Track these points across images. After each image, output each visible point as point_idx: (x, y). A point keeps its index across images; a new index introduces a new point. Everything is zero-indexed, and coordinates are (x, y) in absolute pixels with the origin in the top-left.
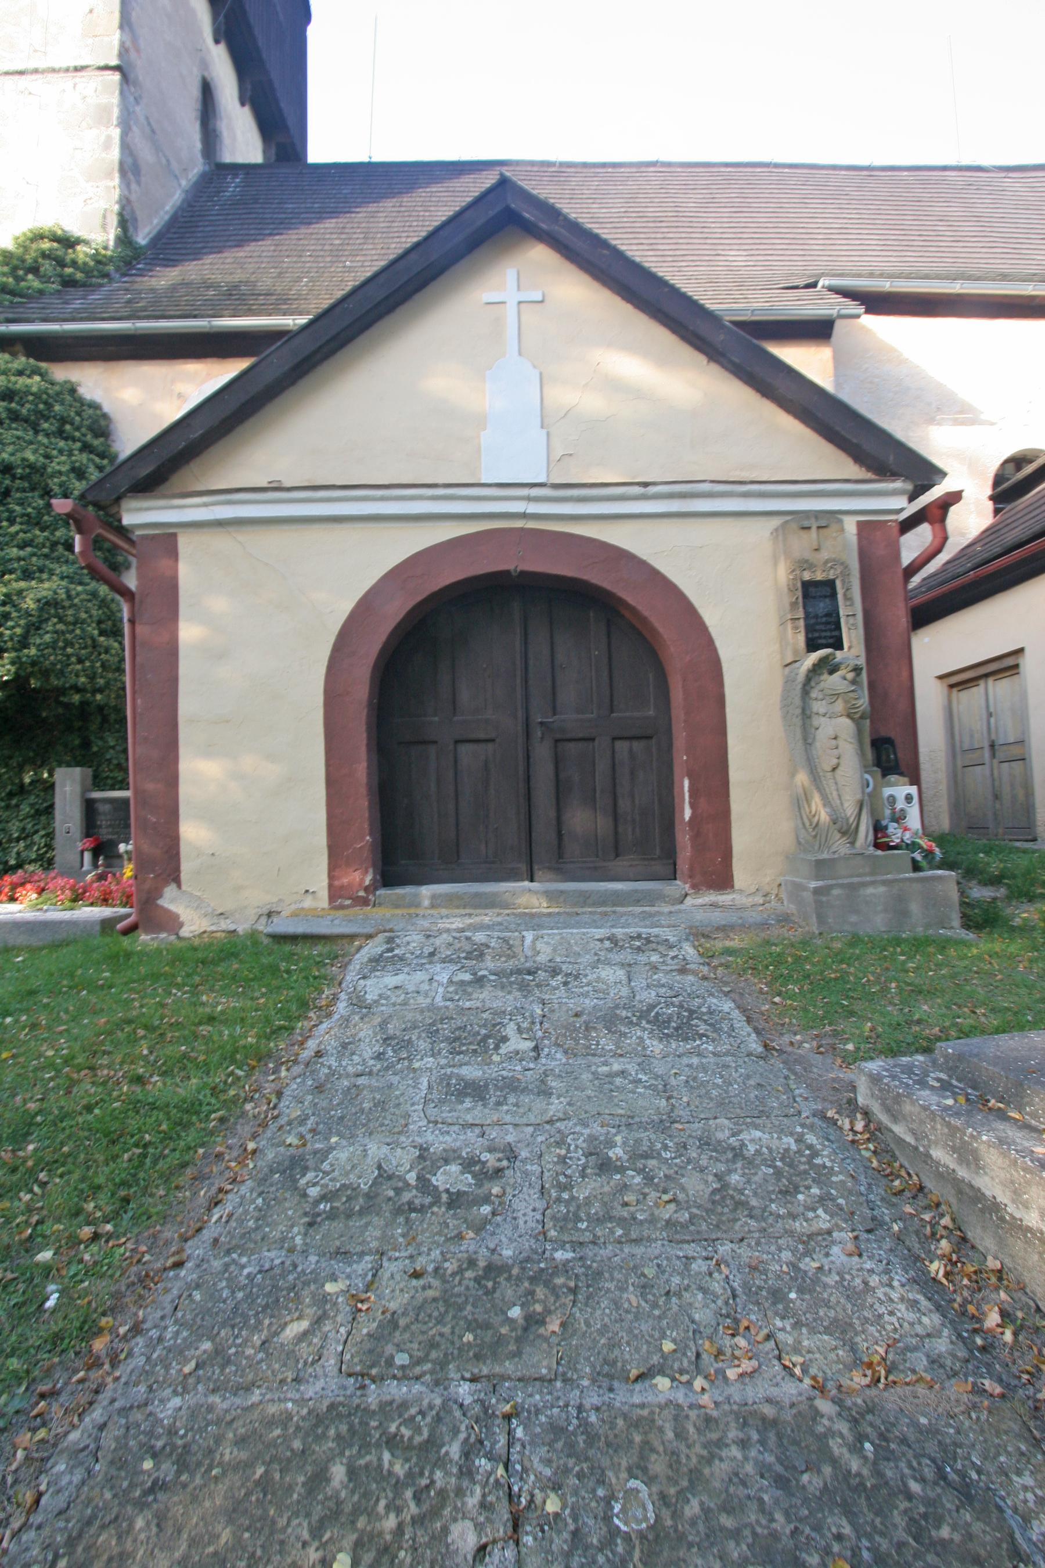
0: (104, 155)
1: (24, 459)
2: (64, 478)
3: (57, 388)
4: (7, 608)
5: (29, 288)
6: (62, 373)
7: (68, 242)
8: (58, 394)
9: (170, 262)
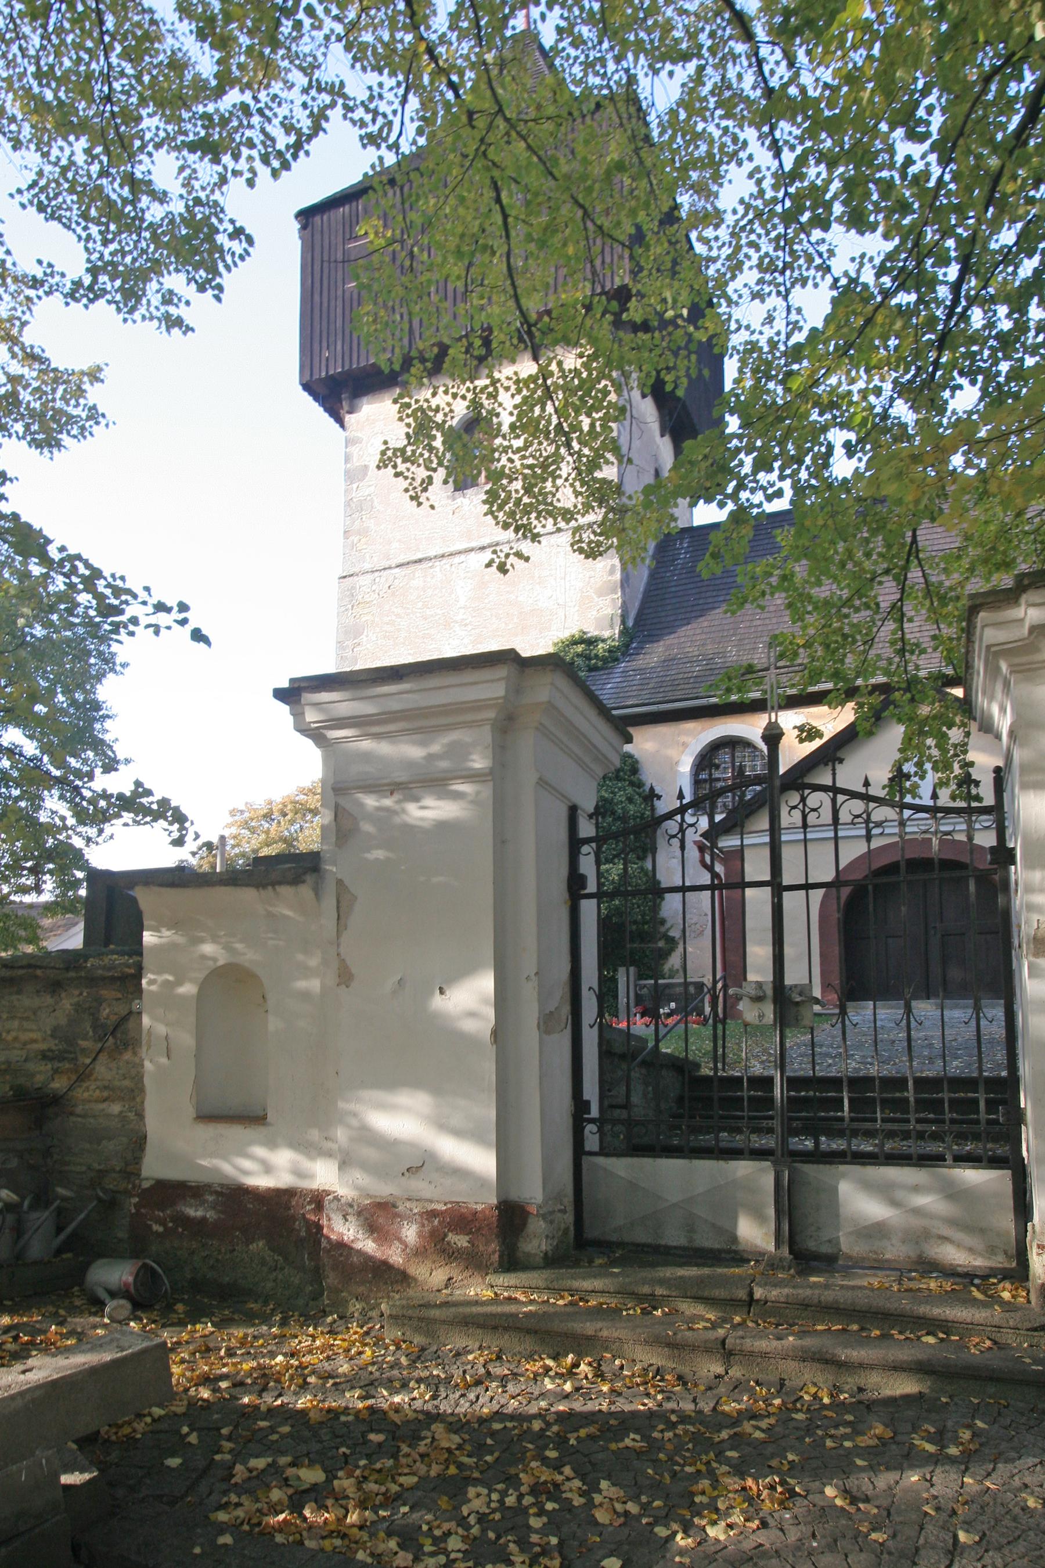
9: (653, 637)
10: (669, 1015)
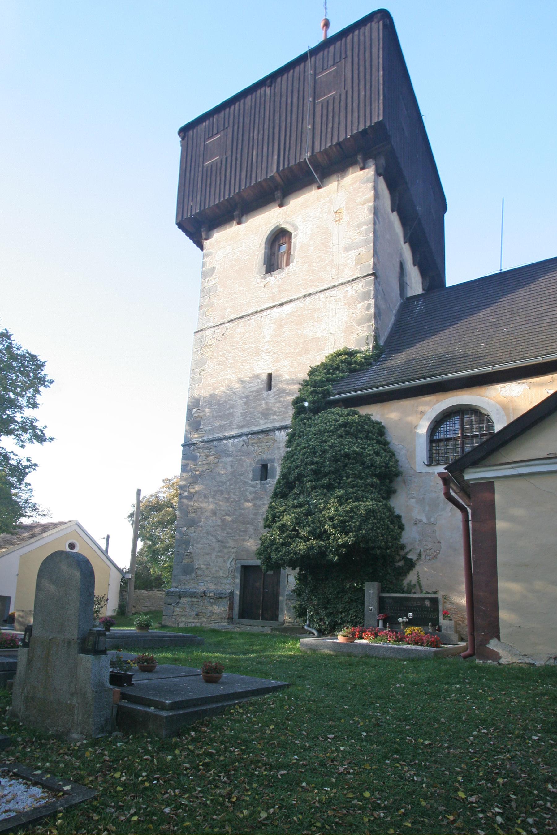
0: (366, 312)
1: (354, 451)
2: (372, 457)
3: (364, 418)
4: (352, 514)
5: (337, 377)
6: (364, 411)
7: (352, 354)
8: (365, 420)
9: (398, 350)
10: (407, 624)
